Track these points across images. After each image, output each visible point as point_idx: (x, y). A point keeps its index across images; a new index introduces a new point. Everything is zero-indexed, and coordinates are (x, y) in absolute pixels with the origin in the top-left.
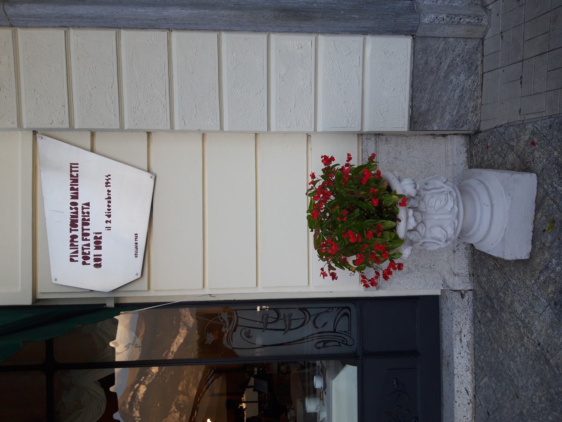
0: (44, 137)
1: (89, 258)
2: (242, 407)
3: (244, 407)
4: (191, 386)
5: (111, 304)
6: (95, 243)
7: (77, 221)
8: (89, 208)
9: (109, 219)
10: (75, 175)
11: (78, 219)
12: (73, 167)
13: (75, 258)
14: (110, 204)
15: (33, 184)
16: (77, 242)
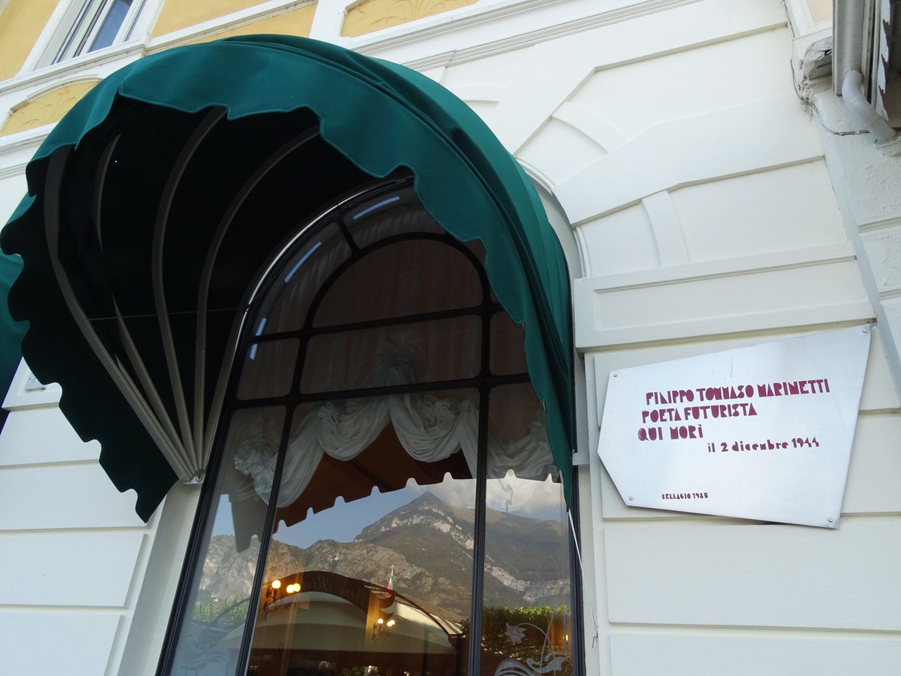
0: (869, 336)
4: (443, 596)
5: (577, 459)
7: (719, 397)
8: (745, 414)
9: (729, 447)
10: (805, 389)
11: (720, 400)
12: (822, 385)
13: (653, 400)
14: (759, 448)
15: (769, 329)
16: (682, 401)
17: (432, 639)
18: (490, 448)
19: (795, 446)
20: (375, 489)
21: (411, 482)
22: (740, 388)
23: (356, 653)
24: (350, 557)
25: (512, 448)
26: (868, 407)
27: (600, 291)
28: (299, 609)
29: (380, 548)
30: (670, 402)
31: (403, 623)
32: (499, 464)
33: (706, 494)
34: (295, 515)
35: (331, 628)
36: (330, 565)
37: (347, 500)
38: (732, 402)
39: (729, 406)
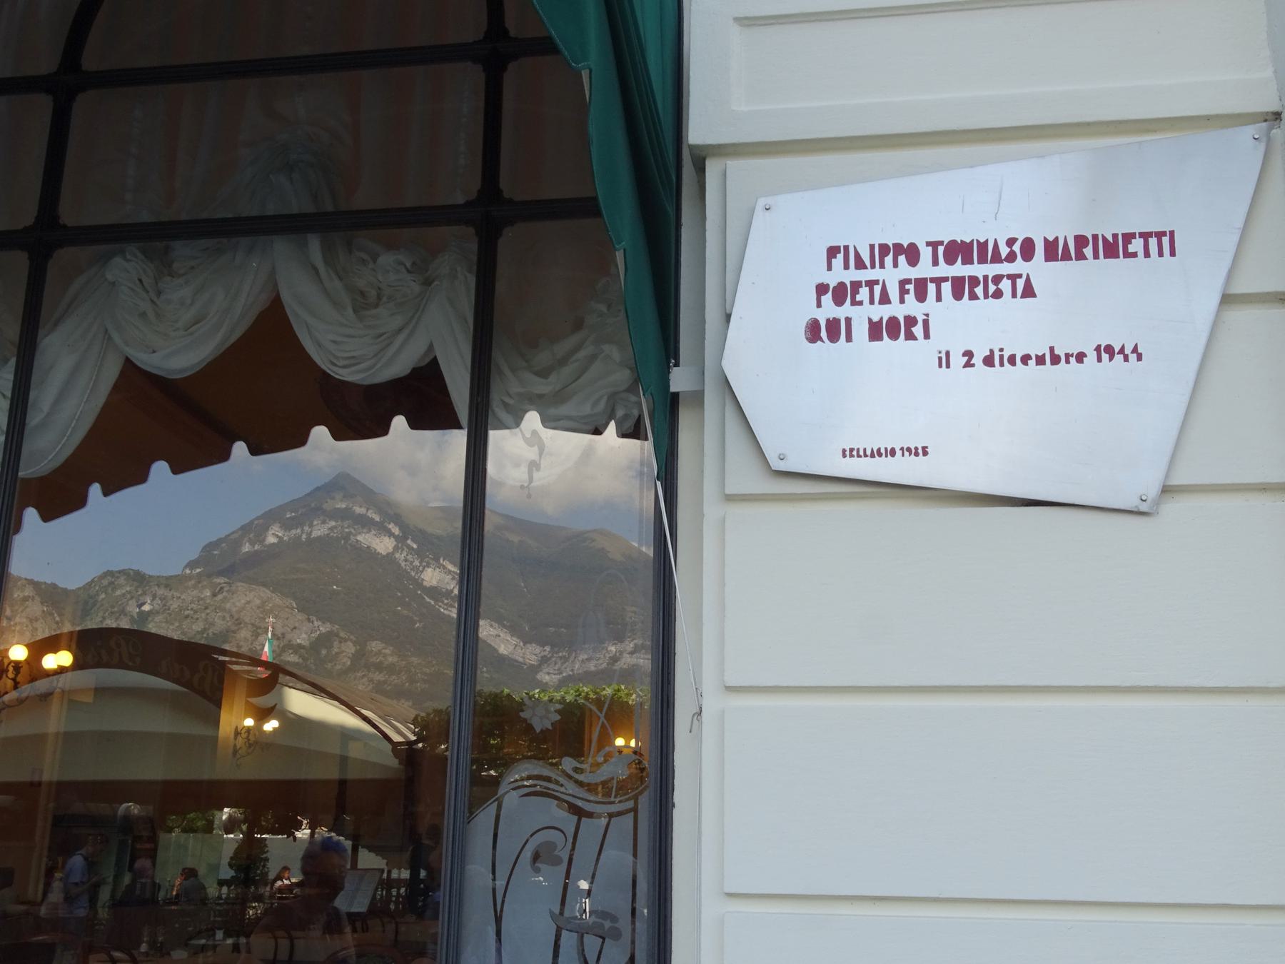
0: (1262, 147)
1: (839, 301)
2: (298, 826)
3: (298, 835)
4: (378, 677)
5: (679, 380)
6: (893, 322)
7: (968, 261)
8: (1014, 295)
9: (978, 360)
10: (1131, 249)
11: (971, 265)
12: (1164, 241)
14: (1032, 362)
16: (896, 265)
17: (355, 751)
18: (497, 356)
19: (1099, 359)
20: (240, 448)
21: (320, 433)
22: (1010, 242)
23: (199, 783)
24: (174, 605)
25: (543, 357)
26: (1240, 288)
27: (747, 22)
28: (70, 701)
29: (241, 586)
30: (873, 266)
31: (296, 724)
32: (515, 388)
33: (924, 448)
34: (60, 496)
35: (144, 737)
36: (132, 620)
37: (176, 470)
38: (991, 270)
39: (986, 277)
